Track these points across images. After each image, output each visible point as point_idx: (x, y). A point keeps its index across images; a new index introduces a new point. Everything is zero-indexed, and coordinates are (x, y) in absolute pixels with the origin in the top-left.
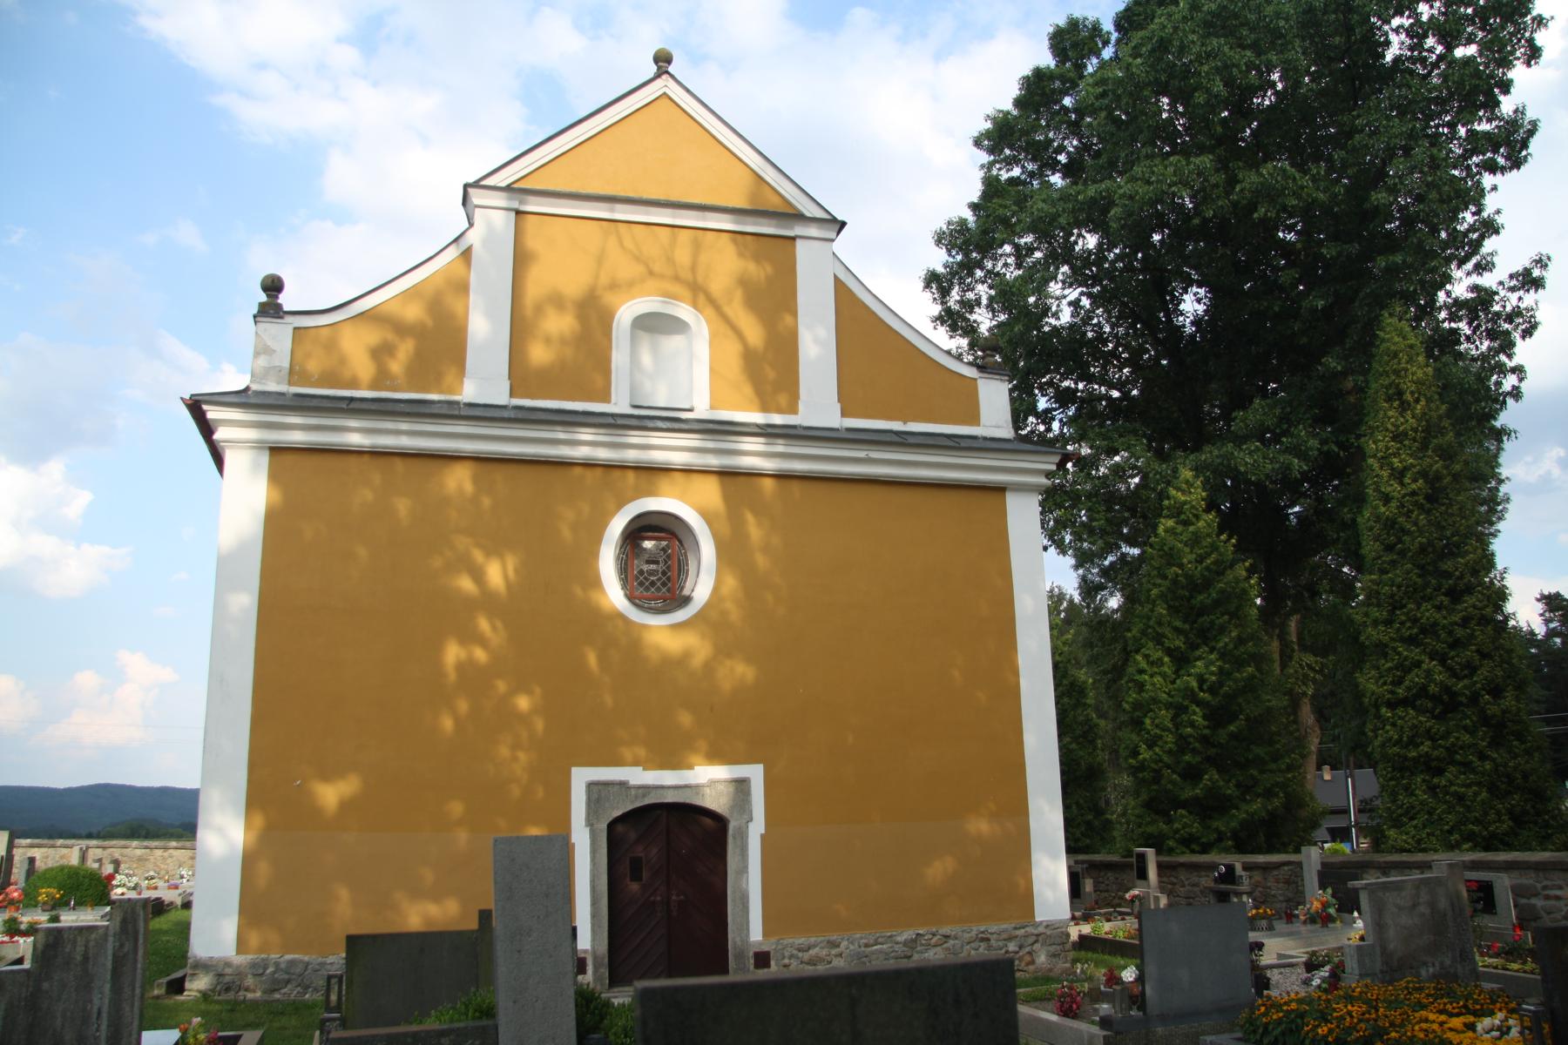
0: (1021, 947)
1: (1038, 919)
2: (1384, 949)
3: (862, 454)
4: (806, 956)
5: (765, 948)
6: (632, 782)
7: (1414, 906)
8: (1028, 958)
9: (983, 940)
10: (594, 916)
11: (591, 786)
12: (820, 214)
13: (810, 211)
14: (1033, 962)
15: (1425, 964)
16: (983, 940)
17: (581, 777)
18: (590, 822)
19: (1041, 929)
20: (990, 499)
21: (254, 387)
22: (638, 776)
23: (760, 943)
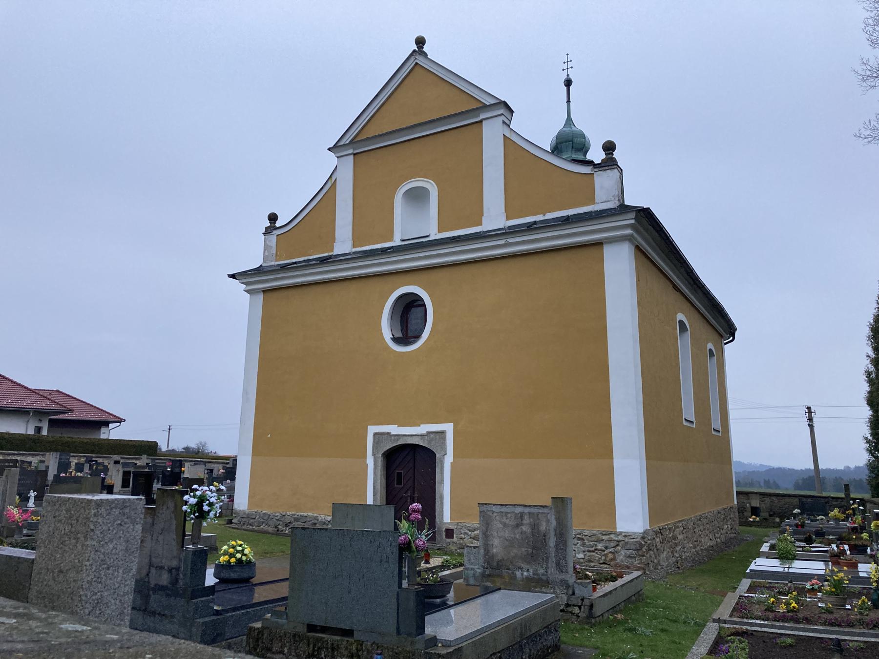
0: (606, 548)
1: (618, 530)
2: (487, 551)
3: (503, 242)
4: (473, 534)
5: (451, 527)
6: (393, 433)
7: (517, 526)
8: (610, 556)
9: (579, 539)
10: (442, 504)
11: (375, 434)
12: (493, 101)
13: (489, 101)
14: (614, 559)
15: (521, 569)
16: (579, 539)
17: (372, 430)
18: (374, 454)
19: (620, 538)
20: (593, 251)
21: (264, 265)
22: (394, 429)
23: (449, 524)
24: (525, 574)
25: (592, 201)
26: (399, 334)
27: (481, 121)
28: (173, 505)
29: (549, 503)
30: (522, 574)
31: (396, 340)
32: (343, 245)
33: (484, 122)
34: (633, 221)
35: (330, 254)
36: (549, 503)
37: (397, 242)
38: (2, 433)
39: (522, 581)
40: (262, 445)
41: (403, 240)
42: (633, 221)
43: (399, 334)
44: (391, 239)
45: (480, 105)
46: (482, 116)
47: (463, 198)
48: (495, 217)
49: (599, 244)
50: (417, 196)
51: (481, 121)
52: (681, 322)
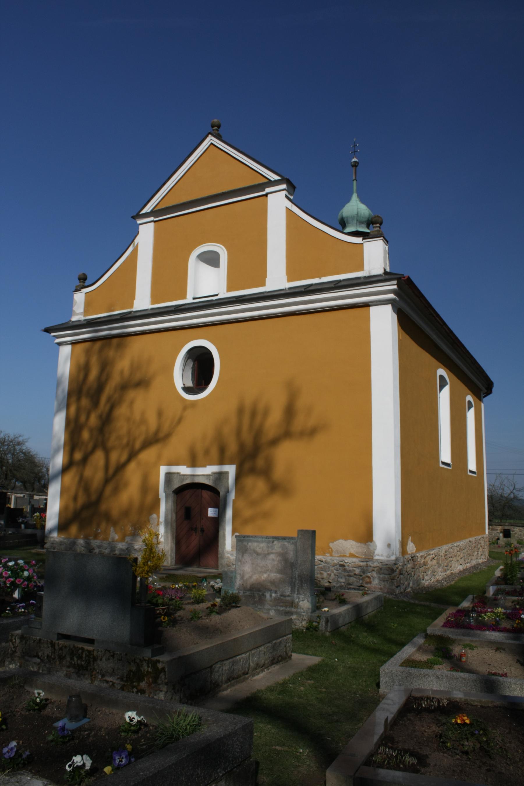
24: (273, 595)
25: (361, 267)
26: (190, 384)
27: (266, 195)
28: (259, 550)
29: (295, 534)
30: (271, 596)
31: (187, 390)
32: (142, 301)
33: (269, 196)
34: (395, 287)
35: (129, 310)
36: (295, 534)
37: (189, 300)
38: (1, 442)
39: (271, 601)
40: (452, 462)
41: (194, 299)
42: (395, 287)
43: (190, 384)
44: (185, 297)
45: (267, 181)
46: (268, 190)
47: (248, 262)
48: (277, 278)
49: (367, 305)
50: (211, 259)
51: (266, 195)
52: (441, 377)
